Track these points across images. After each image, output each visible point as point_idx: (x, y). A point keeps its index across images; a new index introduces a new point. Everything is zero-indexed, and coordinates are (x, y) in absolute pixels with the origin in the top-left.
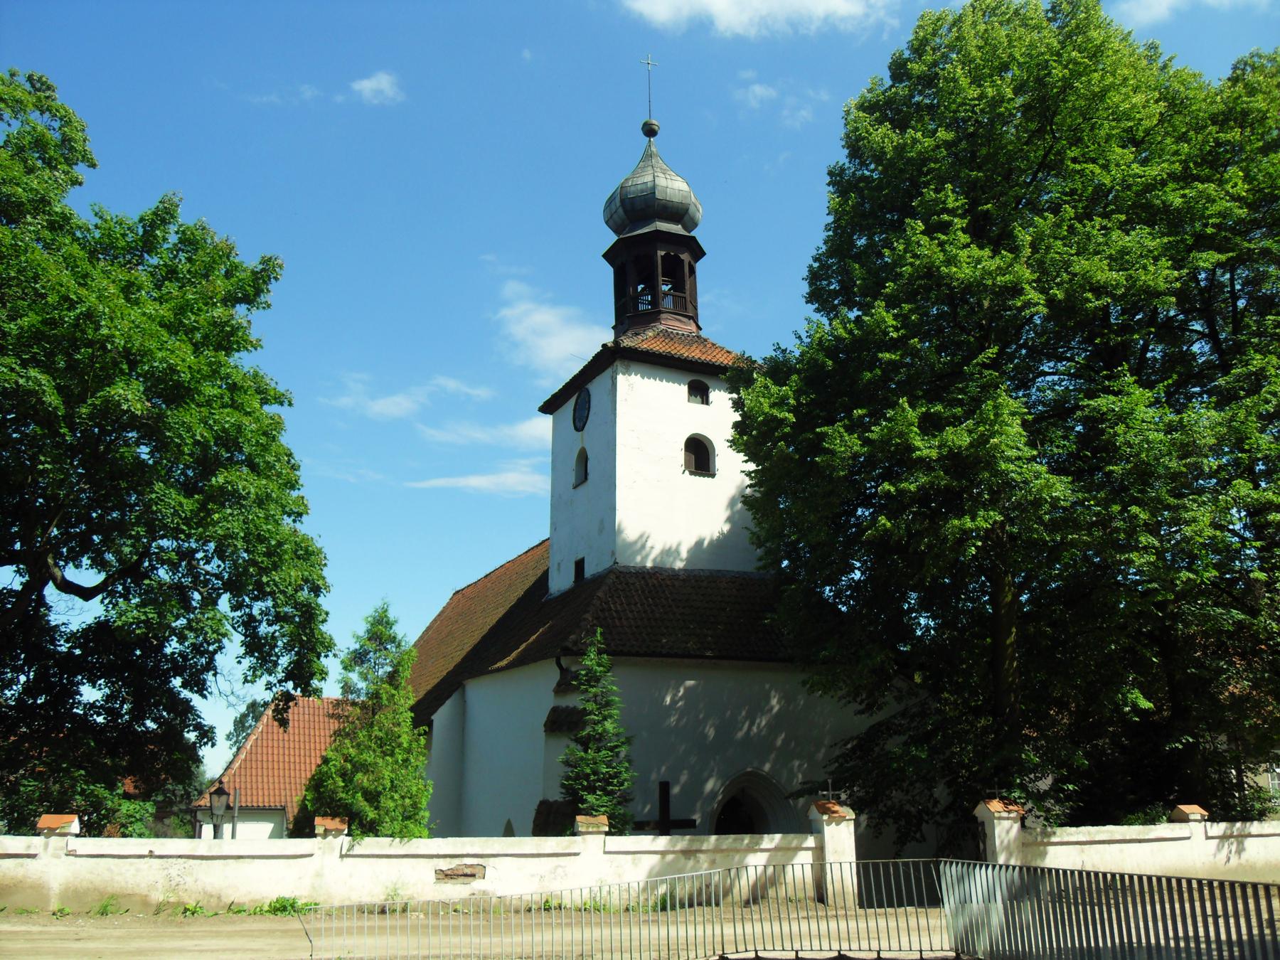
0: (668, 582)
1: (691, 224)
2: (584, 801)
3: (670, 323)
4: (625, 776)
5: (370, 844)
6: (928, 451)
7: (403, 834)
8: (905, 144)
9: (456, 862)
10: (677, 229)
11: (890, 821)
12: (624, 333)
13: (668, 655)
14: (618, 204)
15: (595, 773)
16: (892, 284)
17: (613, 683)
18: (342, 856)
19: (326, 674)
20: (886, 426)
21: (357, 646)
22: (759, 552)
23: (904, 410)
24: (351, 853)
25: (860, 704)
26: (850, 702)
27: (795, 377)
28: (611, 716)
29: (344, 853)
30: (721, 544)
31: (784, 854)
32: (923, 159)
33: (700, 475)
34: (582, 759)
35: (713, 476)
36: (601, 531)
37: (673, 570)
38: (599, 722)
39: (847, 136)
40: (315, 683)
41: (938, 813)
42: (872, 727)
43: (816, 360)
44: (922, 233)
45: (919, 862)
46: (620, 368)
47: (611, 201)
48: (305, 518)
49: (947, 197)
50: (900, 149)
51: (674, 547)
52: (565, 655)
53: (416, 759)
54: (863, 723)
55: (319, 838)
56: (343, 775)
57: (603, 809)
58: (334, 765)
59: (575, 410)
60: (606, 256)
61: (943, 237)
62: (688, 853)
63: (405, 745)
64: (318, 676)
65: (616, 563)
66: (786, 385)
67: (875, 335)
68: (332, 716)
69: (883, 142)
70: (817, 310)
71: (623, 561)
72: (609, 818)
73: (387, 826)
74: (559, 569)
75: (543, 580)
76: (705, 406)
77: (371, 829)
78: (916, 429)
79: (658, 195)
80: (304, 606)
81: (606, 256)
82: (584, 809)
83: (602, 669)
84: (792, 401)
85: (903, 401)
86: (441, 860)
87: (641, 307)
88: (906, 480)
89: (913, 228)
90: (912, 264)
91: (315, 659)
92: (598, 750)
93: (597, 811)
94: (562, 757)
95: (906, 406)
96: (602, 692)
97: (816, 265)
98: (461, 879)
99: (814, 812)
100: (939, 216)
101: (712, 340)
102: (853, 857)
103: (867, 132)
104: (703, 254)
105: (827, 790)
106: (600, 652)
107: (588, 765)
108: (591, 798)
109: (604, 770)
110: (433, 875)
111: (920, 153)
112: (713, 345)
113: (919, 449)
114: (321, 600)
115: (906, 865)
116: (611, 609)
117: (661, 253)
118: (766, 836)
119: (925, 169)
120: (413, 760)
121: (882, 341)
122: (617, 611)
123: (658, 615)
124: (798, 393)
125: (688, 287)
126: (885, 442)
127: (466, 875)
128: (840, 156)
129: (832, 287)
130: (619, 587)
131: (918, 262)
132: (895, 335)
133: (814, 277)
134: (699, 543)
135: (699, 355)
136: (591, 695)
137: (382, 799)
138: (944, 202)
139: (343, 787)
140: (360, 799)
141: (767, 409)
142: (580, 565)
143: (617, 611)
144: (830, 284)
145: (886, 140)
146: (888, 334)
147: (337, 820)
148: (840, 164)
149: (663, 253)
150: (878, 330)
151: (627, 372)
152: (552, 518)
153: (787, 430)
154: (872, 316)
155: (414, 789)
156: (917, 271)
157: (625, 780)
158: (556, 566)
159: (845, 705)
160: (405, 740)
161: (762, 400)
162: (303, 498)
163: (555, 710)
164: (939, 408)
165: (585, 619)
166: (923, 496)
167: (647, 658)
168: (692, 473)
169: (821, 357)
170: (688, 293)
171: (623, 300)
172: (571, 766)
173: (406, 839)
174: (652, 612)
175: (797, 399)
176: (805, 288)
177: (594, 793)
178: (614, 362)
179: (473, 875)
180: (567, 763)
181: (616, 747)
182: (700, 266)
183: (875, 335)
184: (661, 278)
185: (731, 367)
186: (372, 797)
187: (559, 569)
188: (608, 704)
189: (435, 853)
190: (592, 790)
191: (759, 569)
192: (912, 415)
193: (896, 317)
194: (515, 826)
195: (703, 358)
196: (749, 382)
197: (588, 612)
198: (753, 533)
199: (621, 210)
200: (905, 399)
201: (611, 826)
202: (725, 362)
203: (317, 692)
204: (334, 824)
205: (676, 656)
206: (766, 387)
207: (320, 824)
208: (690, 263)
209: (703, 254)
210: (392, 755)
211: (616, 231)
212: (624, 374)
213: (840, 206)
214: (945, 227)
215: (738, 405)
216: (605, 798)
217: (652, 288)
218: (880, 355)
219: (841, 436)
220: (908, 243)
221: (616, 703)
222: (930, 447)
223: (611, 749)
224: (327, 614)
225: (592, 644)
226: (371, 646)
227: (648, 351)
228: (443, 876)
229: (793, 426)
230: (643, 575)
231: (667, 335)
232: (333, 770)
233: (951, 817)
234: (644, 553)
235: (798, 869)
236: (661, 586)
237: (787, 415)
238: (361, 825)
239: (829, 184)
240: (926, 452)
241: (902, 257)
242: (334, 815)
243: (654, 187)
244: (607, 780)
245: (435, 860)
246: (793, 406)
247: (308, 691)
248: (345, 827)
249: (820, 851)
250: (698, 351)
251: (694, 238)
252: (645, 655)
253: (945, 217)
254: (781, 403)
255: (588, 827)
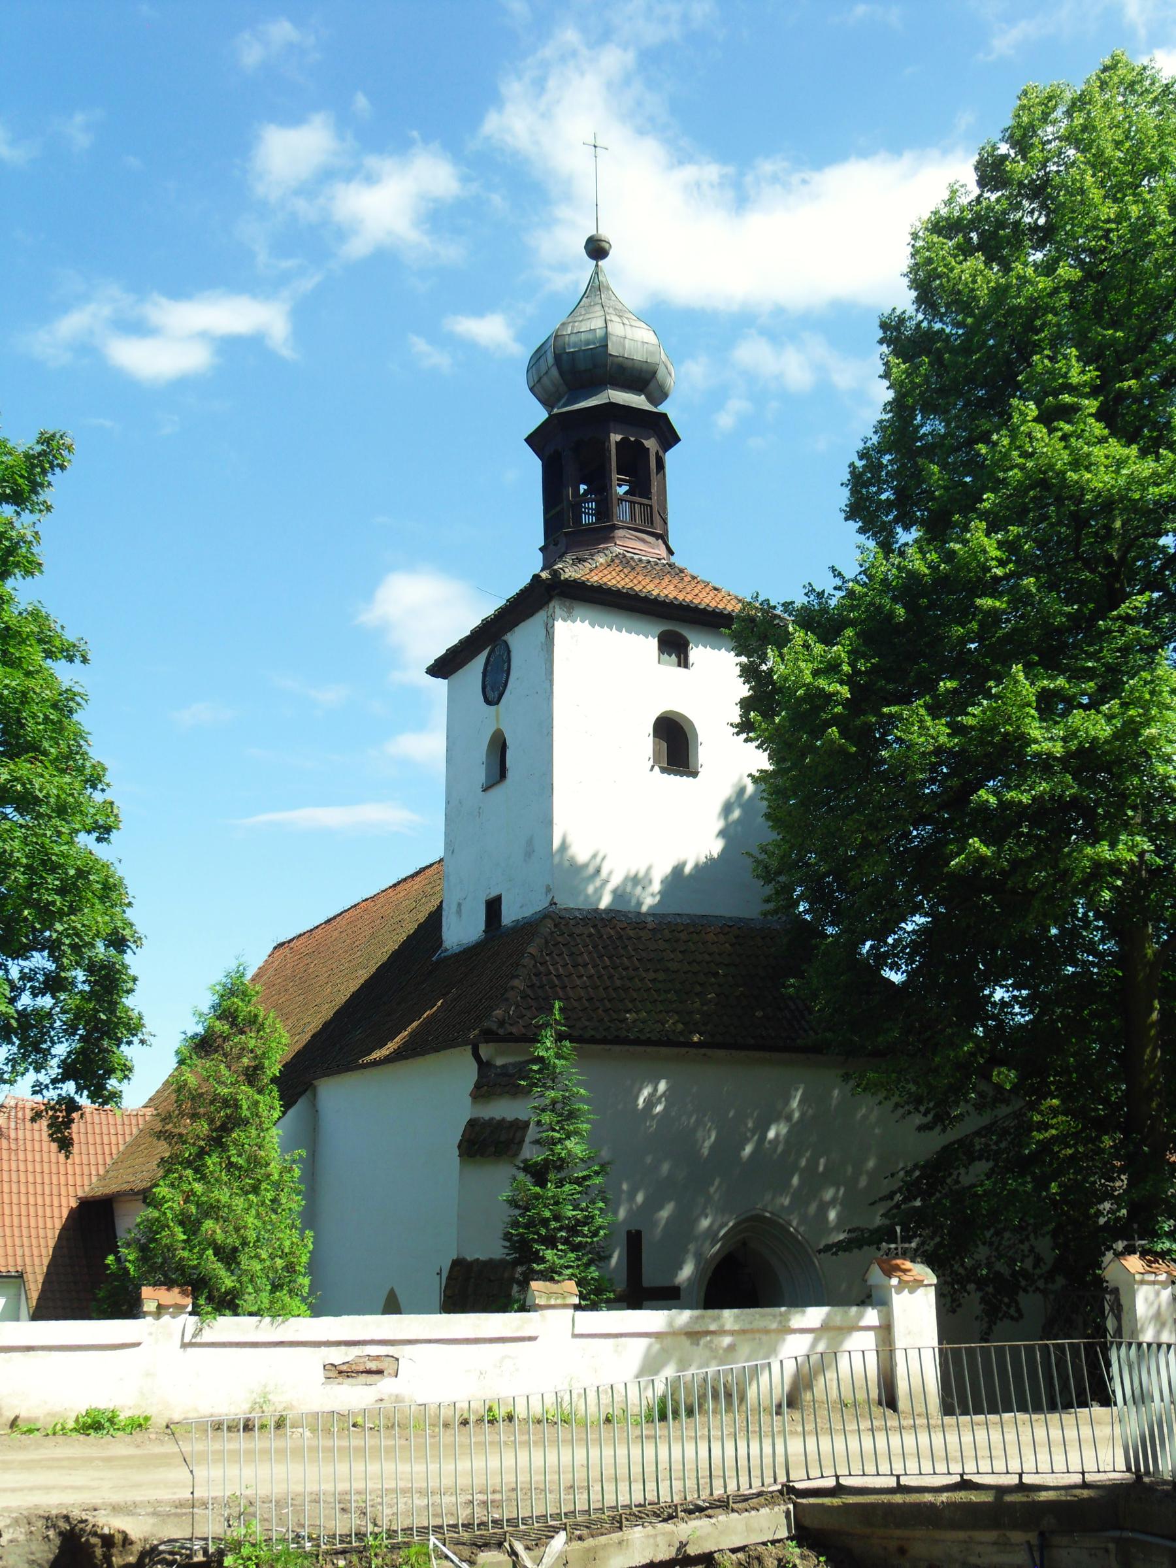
0: (631, 933)
1: (659, 394)
2: (543, 1260)
3: (628, 543)
4: (599, 1221)
5: (226, 1326)
6: (1050, 744)
7: (276, 1311)
8: (1009, 286)
9: (355, 1352)
10: (637, 401)
11: (971, 1287)
12: (561, 557)
13: (637, 1042)
14: (550, 359)
15: (557, 1218)
16: (992, 496)
17: (580, 1083)
18: (184, 1345)
19: (130, 1070)
20: (990, 707)
21: (200, 1029)
22: (769, 890)
23: (1016, 682)
24: (198, 1340)
25: (925, 1115)
26: (909, 1113)
27: (849, 632)
28: (577, 1133)
29: (187, 1340)
30: (708, 870)
31: (833, 1332)
32: (1036, 308)
33: (676, 773)
34: (537, 1197)
35: (694, 774)
36: (529, 853)
37: (596, 910)
38: (560, 1141)
39: (914, 269)
40: (112, 1083)
41: (1040, 1277)
42: (945, 1148)
43: (880, 608)
44: (1035, 420)
45: (1063, 1344)
46: (558, 611)
47: (539, 355)
48: (114, 835)
49: (1069, 367)
50: (1000, 293)
51: (641, 874)
52: (487, 1042)
53: (289, 1199)
54: (936, 1141)
55: (149, 1319)
56: (184, 1221)
57: (569, 1271)
58: (171, 1208)
59: (485, 673)
60: (530, 440)
61: (1067, 428)
62: (693, 1335)
63: (276, 1177)
64: (119, 1074)
65: (553, 903)
66: (837, 644)
67: (969, 571)
68: (160, 1135)
69: (974, 282)
70: (862, 531)
71: (566, 901)
72: (578, 1284)
73: (248, 1301)
74: (459, 912)
75: (433, 923)
76: (682, 670)
77: (228, 1304)
78: (1033, 712)
79: (612, 350)
80: (103, 967)
81: (530, 440)
82: (541, 1272)
83: (563, 1062)
84: (846, 668)
85: (1017, 669)
86: (333, 1349)
87: (585, 519)
88: (1017, 787)
89: (1022, 413)
90: (1022, 468)
91: (115, 1049)
92: (560, 1184)
93: (560, 1274)
94: (506, 1194)
95: (1021, 676)
96: (564, 1097)
97: (860, 464)
98: (363, 1378)
99: (875, 1274)
100: (1056, 396)
101: (691, 570)
102: (935, 1342)
103: (945, 266)
104: (677, 439)
105: (896, 1243)
106: (560, 1037)
107: (546, 1206)
108: (549, 1254)
109: (570, 1214)
110: (320, 1374)
111: (1031, 299)
112: (694, 578)
113: (1036, 742)
114: (128, 958)
115: (1060, 1348)
116: (549, 973)
117: (616, 438)
118: (870, 1308)
119: (1038, 323)
120: (284, 1201)
121: (979, 579)
122: (558, 976)
123: (618, 983)
124: (854, 654)
125: (654, 490)
126: (987, 729)
127: (369, 1372)
128: (904, 300)
129: (883, 497)
130: (560, 939)
131: (1030, 464)
132: (999, 572)
133: (858, 481)
134: (678, 870)
135: (674, 594)
136: (548, 1101)
137: (243, 1258)
138: (1065, 376)
139: (184, 1241)
140: (213, 1258)
141: (808, 678)
142: (493, 907)
143: (558, 976)
144: (881, 491)
145: (979, 279)
146: (989, 569)
147: (176, 1290)
148: (898, 312)
149: (618, 438)
150: (974, 564)
151: (569, 617)
152: (447, 835)
153: (838, 709)
154: (965, 542)
155: (287, 1243)
156: (1029, 478)
157: (601, 1228)
158: (454, 908)
159: (903, 1117)
160: (274, 1169)
161: (802, 665)
162: (112, 803)
163: (472, 1124)
164: (1061, 681)
165: (513, 988)
166: (1040, 811)
167: (607, 1047)
168: (663, 770)
169: (886, 601)
170: (655, 498)
171: (558, 509)
172: (517, 1207)
173: (280, 1319)
174: (611, 977)
175: (852, 664)
176: (843, 496)
177: (554, 1247)
178: (547, 603)
179: (380, 1372)
180: (513, 1203)
181: (585, 1178)
182: (670, 457)
183: (969, 571)
184: (615, 476)
185: (738, 617)
186: (229, 1256)
187: (459, 912)
188: (572, 1115)
189: (324, 1339)
190: (551, 1242)
191: (765, 914)
192: (1028, 690)
193: (1001, 546)
194: (402, 1299)
195: (681, 597)
196: (781, 640)
197: (517, 976)
198: (757, 861)
199: (555, 372)
200: (1020, 666)
201: (582, 1296)
202: (713, 604)
203: (115, 1096)
204: (172, 1296)
205: (648, 1042)
206: (806, 646)
207: (150, 1296)
208: (657, 453)
209: (677, 439)
210: (255, 1189)
211: (547, 403)
212: (564, 620)
213: (909, 375)
214: (1068, 412)
215: (749, 673)
216: (572, 1255)
217: (601, 489)
218: (978, 601)
219: (921, 721)
220: (1014, 433)
221: (584, 1113)
222: (1051, 739)
223: (579, 1181)
224: (135, 979)
225: (546, 1025)
226: (222, 1027)
227: (600, 586)
228: (333, 1374)
229: (846, 704)
230: (597, 921)
231: (625, 562)
232: (169, 1215)
233: (1060, 1281)
234: (598, 883)
235: (857, 1358)
236: (620, 937)
237: (839, 687)
238: (210, 1299)
239: (881, 342)
240: (1046, 746)
241: (1006, 456)
242: (169, 1284)
243: (606, 337)
244: (573, 1230)
245: (324, 1350)
246: (848, 675)
247: (103, 1097)
248: (188, 1301)
249: (886, 1331)
250: (671, 587)
251: (664, 416)
252: (604, 1041)
253: (1067, 398)
254: (831, 668)
255: (549, 1299)
